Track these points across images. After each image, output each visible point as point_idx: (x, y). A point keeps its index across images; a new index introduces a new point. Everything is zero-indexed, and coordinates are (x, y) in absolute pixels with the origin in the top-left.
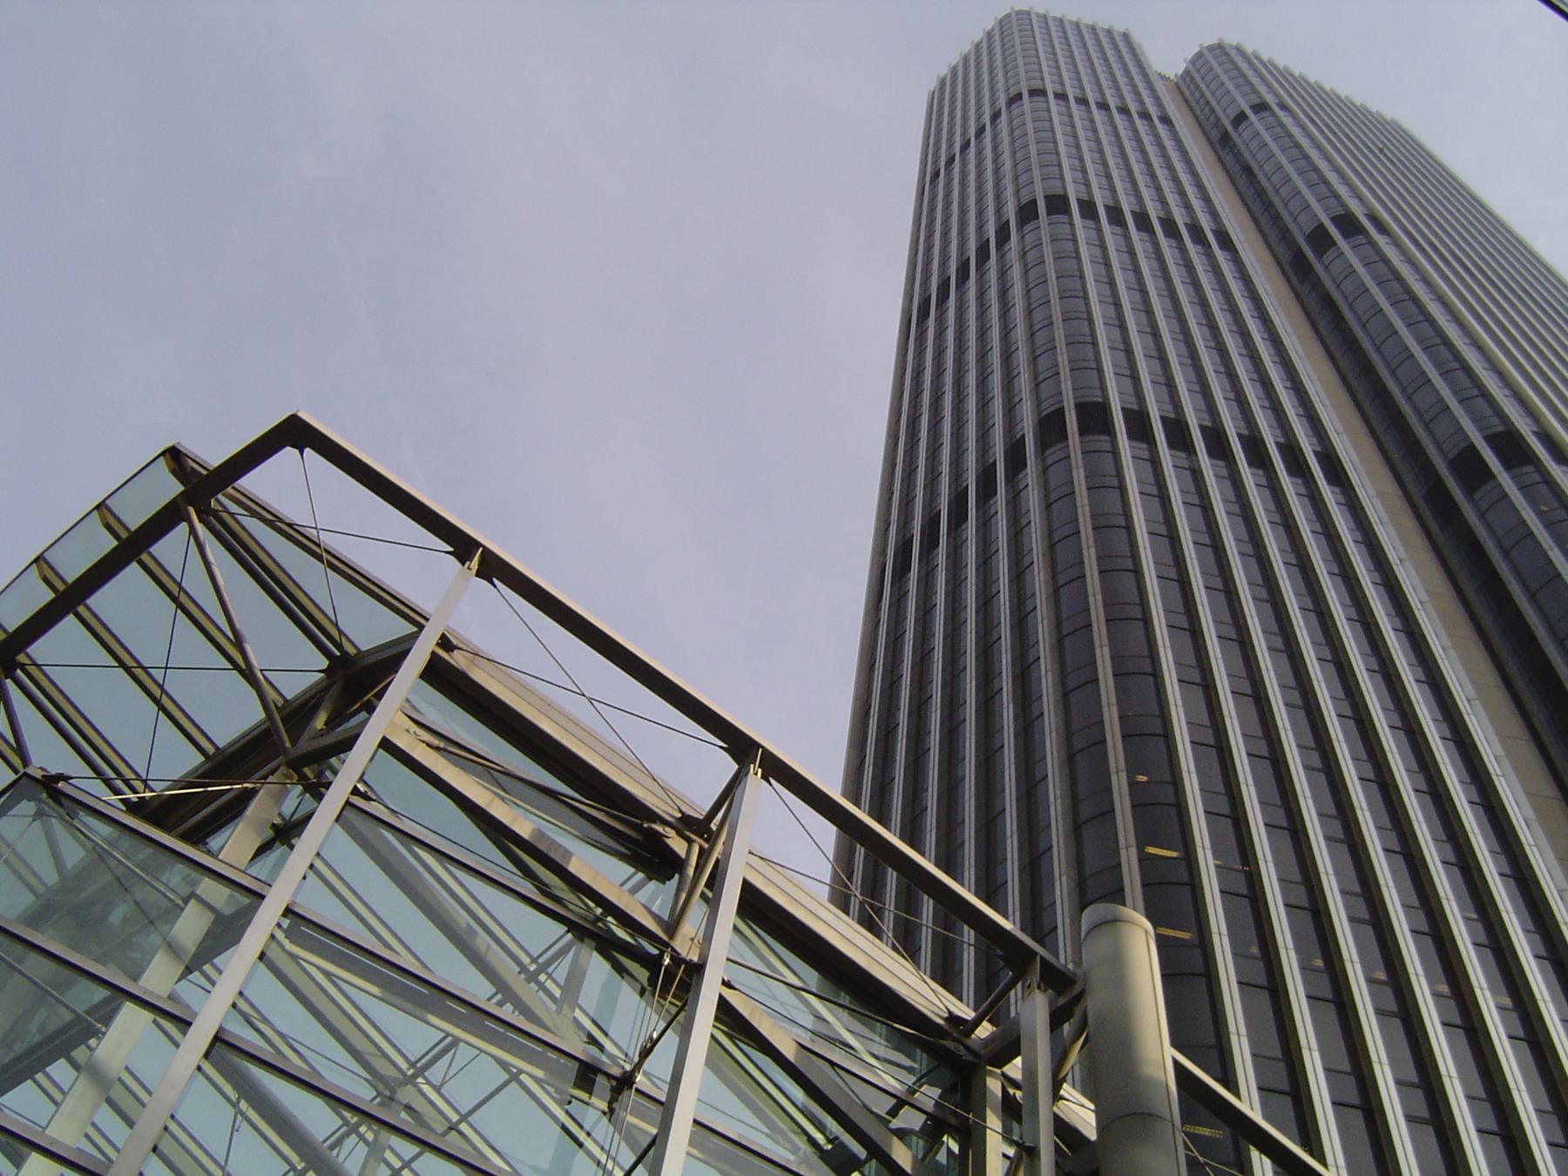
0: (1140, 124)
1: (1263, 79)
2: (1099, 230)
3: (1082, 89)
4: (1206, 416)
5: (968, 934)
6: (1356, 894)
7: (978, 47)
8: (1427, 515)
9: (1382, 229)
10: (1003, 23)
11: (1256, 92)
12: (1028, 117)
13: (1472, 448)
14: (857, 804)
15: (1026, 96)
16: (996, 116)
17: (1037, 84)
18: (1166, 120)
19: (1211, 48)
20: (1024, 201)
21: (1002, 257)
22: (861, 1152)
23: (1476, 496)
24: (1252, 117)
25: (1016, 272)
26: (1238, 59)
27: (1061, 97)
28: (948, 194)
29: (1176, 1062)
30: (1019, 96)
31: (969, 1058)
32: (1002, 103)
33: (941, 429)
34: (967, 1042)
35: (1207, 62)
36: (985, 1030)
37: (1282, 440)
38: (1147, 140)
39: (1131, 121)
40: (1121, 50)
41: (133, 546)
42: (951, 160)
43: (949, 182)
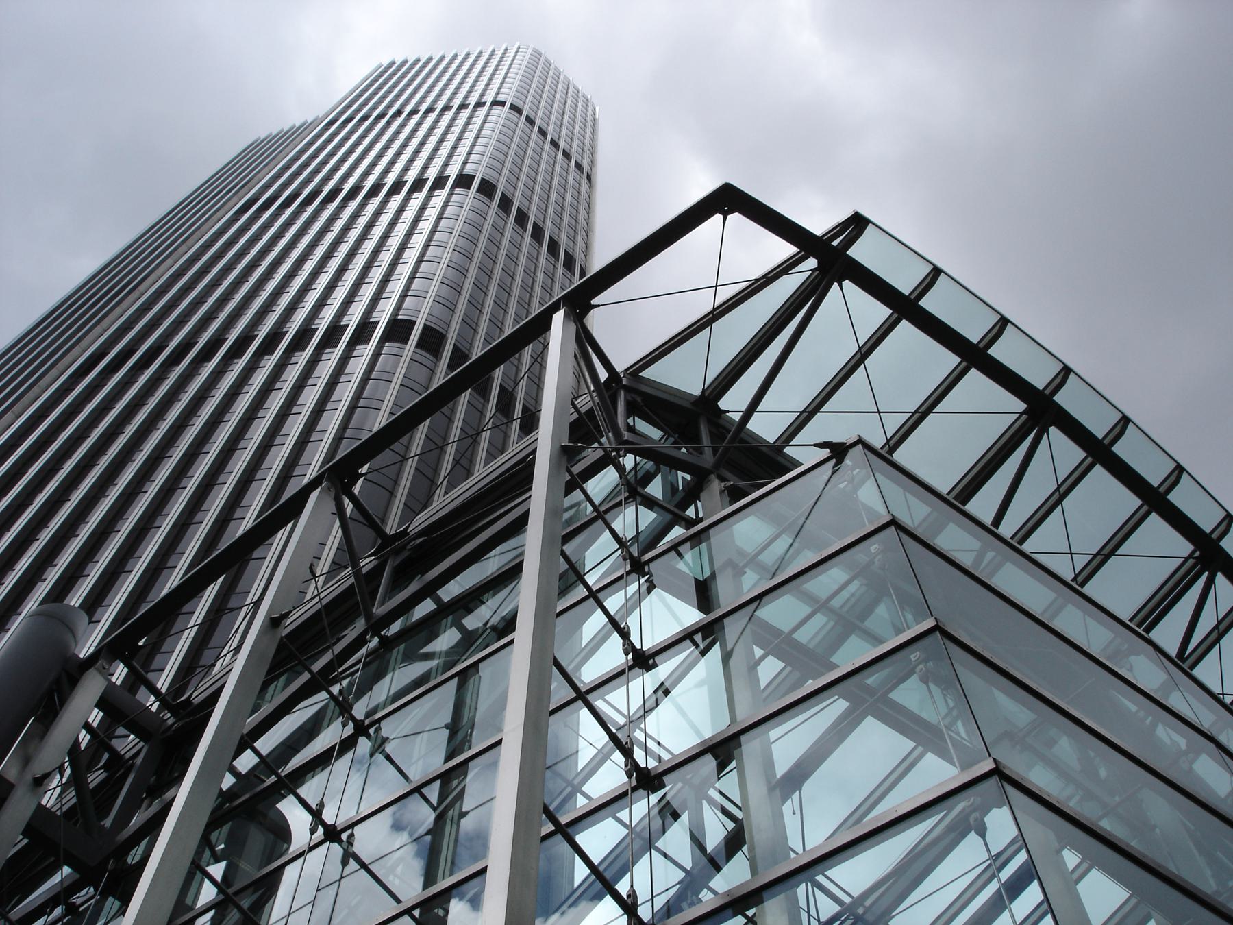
15: (507, 106)
16: (479, 104)
21: (429, 197)
22: (576, 469)
28: (397, 132)
30: (502, 104)
32: (489, 99)
33: (91, 432)
41: (1155, 500)
42: (414, 112)
43: (419, 124)
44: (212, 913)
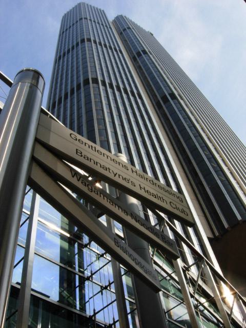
0: (97, 25)
8: (156, 107)
9: (151, 54)
10: (79, 4)
12: (84, 23)
14: (49, 111)
17: (85, 17)
18: (110, 28)
19: (120, 16)
24: (83, 19)
38: (94, 26)
40: (102, 14)
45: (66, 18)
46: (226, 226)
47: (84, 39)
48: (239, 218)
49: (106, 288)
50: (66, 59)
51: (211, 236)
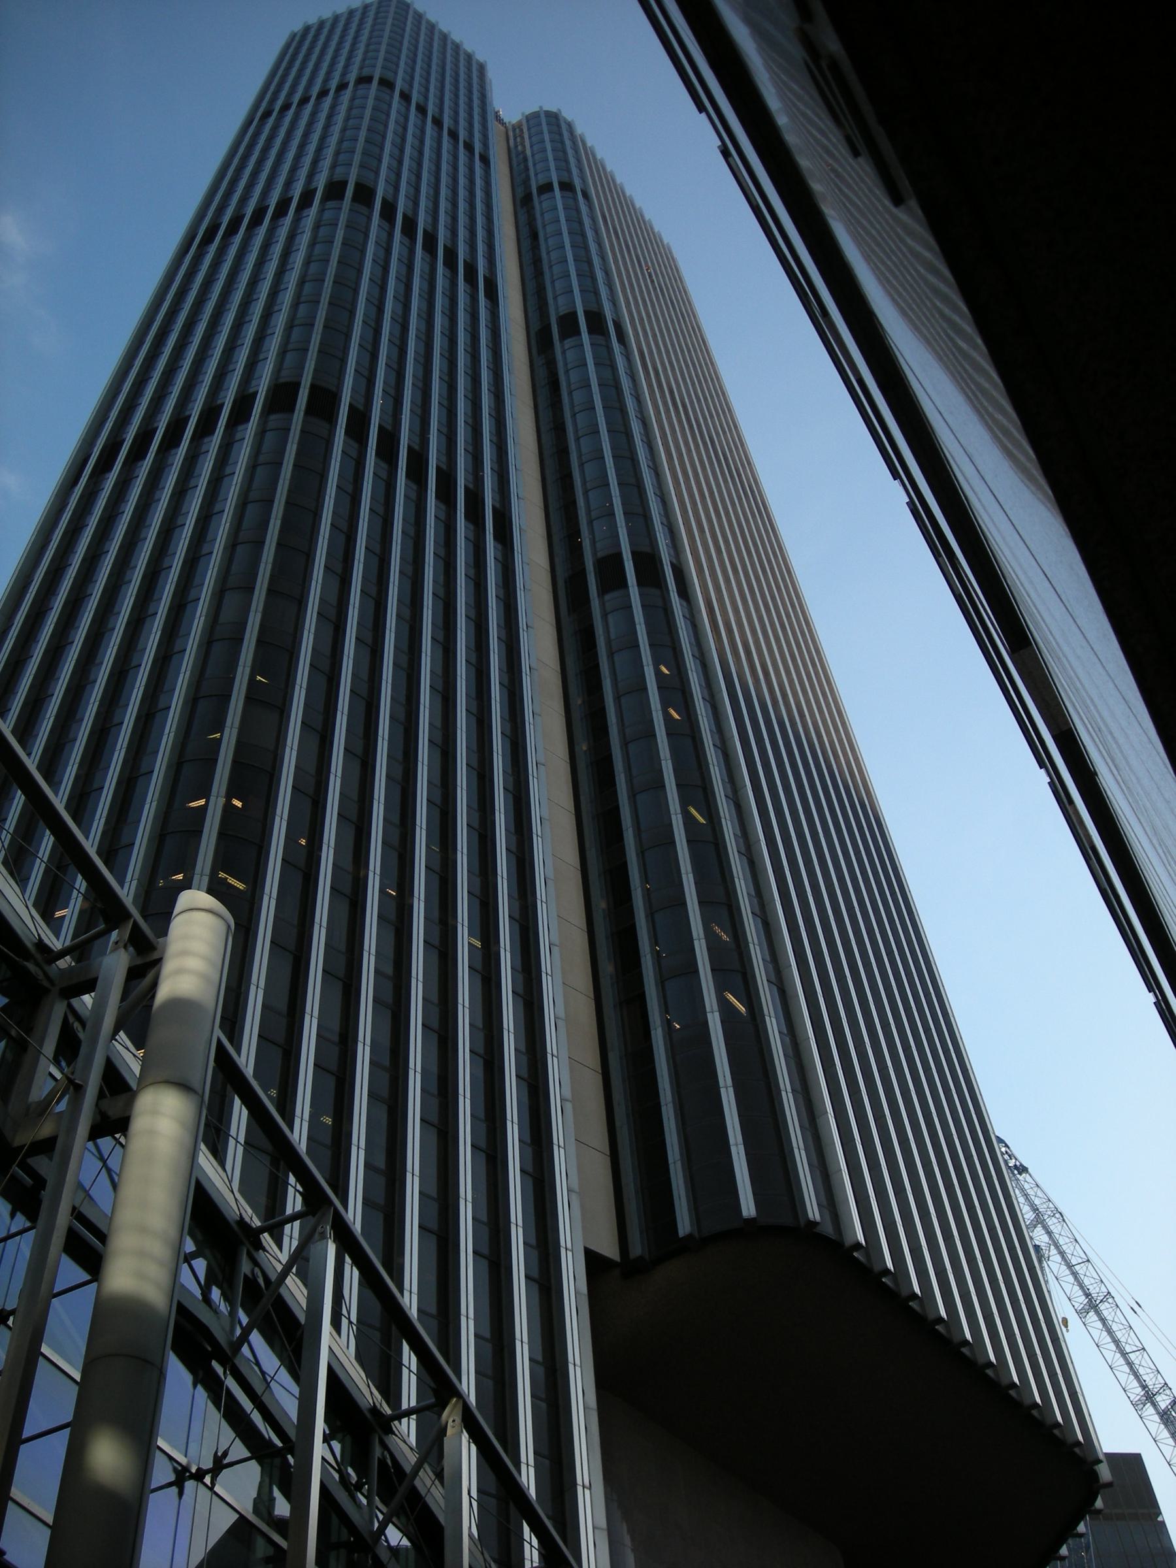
1: (579, 160)
2: (391, 235)
3: (426, 98)
4: (417, 440)
5: (81, 883)
6: (483, 1223)
7: (351, 13)
9: (622, 338)
11: (569, 171)
13: (618, 556)
16: (342, 86)
17: (389, 76)
18: (485, 160)
19: (548, 114)
20: (337, 178)
21: (297, 220)
23: (607, 597)
25: (304, 240)
26: (566, 135)
27: (406, 97)
29: (219, 1042)
31: (46, 983)
32: (352, 78)
34: (46, 968)
35: (540, 124)
36: (65, 963)
37: (471, 486)
39: (456, 147)
40: (470, 77)
44: (348, 1259)
45: (302, 48)
46: (684, 1225)
47: (343, 184)
48: (748, 1207)
49: (199, 1476)
50: (283, 233)
51: (609, 1249)
